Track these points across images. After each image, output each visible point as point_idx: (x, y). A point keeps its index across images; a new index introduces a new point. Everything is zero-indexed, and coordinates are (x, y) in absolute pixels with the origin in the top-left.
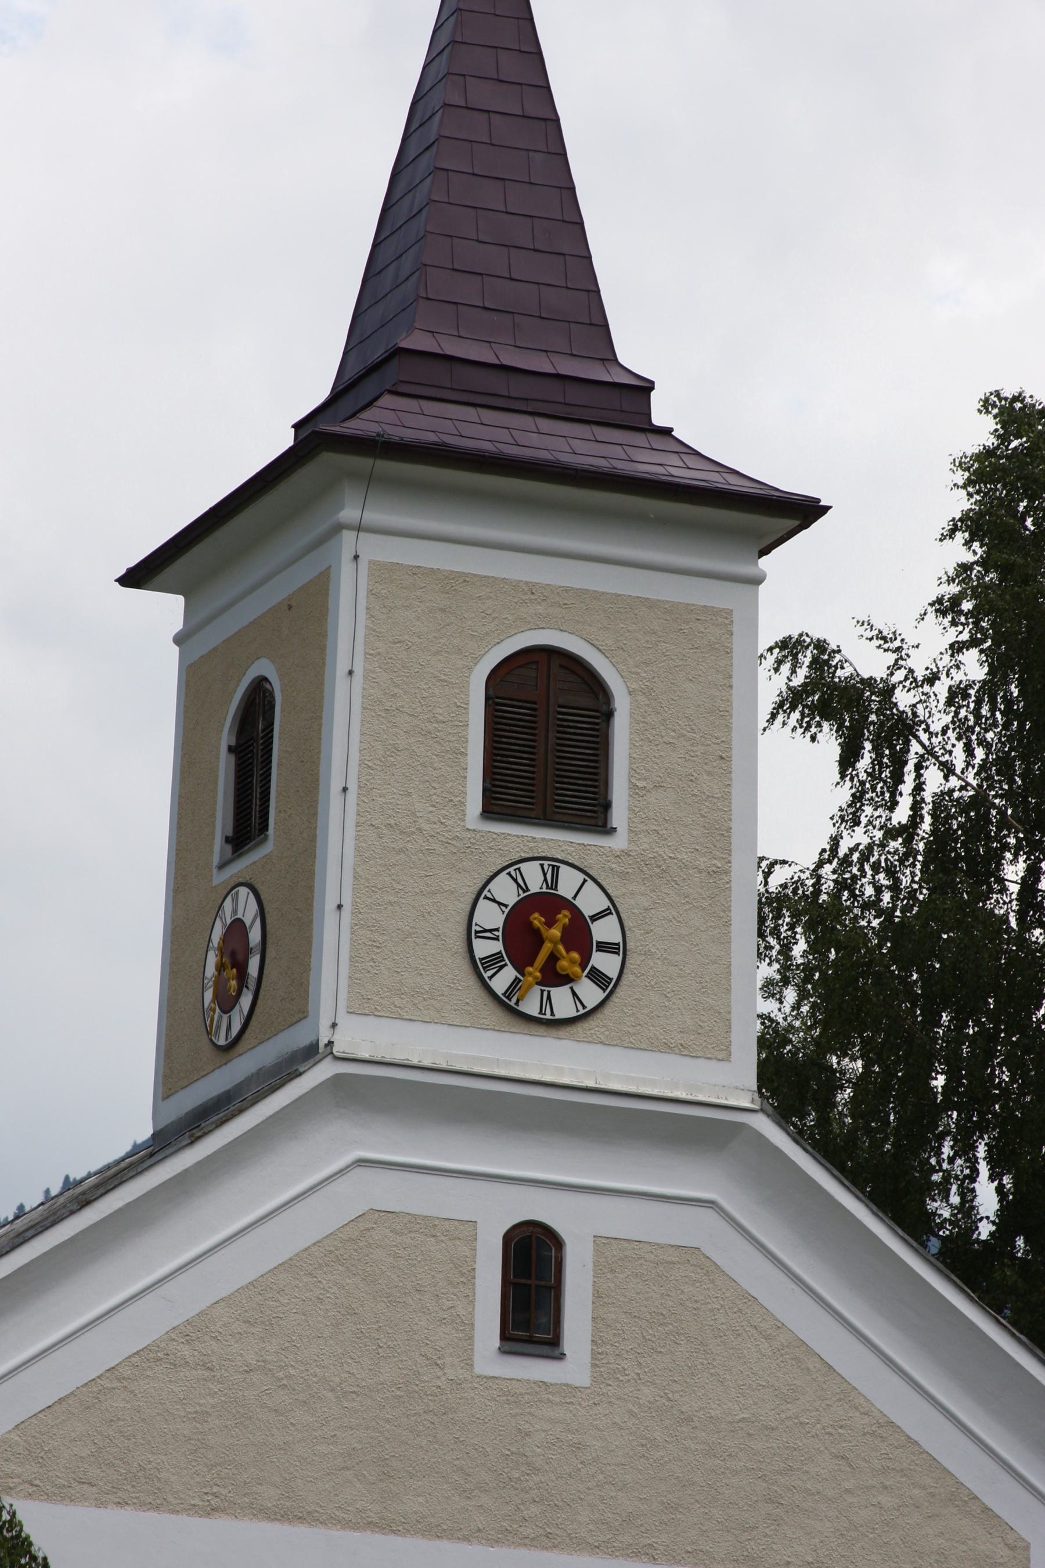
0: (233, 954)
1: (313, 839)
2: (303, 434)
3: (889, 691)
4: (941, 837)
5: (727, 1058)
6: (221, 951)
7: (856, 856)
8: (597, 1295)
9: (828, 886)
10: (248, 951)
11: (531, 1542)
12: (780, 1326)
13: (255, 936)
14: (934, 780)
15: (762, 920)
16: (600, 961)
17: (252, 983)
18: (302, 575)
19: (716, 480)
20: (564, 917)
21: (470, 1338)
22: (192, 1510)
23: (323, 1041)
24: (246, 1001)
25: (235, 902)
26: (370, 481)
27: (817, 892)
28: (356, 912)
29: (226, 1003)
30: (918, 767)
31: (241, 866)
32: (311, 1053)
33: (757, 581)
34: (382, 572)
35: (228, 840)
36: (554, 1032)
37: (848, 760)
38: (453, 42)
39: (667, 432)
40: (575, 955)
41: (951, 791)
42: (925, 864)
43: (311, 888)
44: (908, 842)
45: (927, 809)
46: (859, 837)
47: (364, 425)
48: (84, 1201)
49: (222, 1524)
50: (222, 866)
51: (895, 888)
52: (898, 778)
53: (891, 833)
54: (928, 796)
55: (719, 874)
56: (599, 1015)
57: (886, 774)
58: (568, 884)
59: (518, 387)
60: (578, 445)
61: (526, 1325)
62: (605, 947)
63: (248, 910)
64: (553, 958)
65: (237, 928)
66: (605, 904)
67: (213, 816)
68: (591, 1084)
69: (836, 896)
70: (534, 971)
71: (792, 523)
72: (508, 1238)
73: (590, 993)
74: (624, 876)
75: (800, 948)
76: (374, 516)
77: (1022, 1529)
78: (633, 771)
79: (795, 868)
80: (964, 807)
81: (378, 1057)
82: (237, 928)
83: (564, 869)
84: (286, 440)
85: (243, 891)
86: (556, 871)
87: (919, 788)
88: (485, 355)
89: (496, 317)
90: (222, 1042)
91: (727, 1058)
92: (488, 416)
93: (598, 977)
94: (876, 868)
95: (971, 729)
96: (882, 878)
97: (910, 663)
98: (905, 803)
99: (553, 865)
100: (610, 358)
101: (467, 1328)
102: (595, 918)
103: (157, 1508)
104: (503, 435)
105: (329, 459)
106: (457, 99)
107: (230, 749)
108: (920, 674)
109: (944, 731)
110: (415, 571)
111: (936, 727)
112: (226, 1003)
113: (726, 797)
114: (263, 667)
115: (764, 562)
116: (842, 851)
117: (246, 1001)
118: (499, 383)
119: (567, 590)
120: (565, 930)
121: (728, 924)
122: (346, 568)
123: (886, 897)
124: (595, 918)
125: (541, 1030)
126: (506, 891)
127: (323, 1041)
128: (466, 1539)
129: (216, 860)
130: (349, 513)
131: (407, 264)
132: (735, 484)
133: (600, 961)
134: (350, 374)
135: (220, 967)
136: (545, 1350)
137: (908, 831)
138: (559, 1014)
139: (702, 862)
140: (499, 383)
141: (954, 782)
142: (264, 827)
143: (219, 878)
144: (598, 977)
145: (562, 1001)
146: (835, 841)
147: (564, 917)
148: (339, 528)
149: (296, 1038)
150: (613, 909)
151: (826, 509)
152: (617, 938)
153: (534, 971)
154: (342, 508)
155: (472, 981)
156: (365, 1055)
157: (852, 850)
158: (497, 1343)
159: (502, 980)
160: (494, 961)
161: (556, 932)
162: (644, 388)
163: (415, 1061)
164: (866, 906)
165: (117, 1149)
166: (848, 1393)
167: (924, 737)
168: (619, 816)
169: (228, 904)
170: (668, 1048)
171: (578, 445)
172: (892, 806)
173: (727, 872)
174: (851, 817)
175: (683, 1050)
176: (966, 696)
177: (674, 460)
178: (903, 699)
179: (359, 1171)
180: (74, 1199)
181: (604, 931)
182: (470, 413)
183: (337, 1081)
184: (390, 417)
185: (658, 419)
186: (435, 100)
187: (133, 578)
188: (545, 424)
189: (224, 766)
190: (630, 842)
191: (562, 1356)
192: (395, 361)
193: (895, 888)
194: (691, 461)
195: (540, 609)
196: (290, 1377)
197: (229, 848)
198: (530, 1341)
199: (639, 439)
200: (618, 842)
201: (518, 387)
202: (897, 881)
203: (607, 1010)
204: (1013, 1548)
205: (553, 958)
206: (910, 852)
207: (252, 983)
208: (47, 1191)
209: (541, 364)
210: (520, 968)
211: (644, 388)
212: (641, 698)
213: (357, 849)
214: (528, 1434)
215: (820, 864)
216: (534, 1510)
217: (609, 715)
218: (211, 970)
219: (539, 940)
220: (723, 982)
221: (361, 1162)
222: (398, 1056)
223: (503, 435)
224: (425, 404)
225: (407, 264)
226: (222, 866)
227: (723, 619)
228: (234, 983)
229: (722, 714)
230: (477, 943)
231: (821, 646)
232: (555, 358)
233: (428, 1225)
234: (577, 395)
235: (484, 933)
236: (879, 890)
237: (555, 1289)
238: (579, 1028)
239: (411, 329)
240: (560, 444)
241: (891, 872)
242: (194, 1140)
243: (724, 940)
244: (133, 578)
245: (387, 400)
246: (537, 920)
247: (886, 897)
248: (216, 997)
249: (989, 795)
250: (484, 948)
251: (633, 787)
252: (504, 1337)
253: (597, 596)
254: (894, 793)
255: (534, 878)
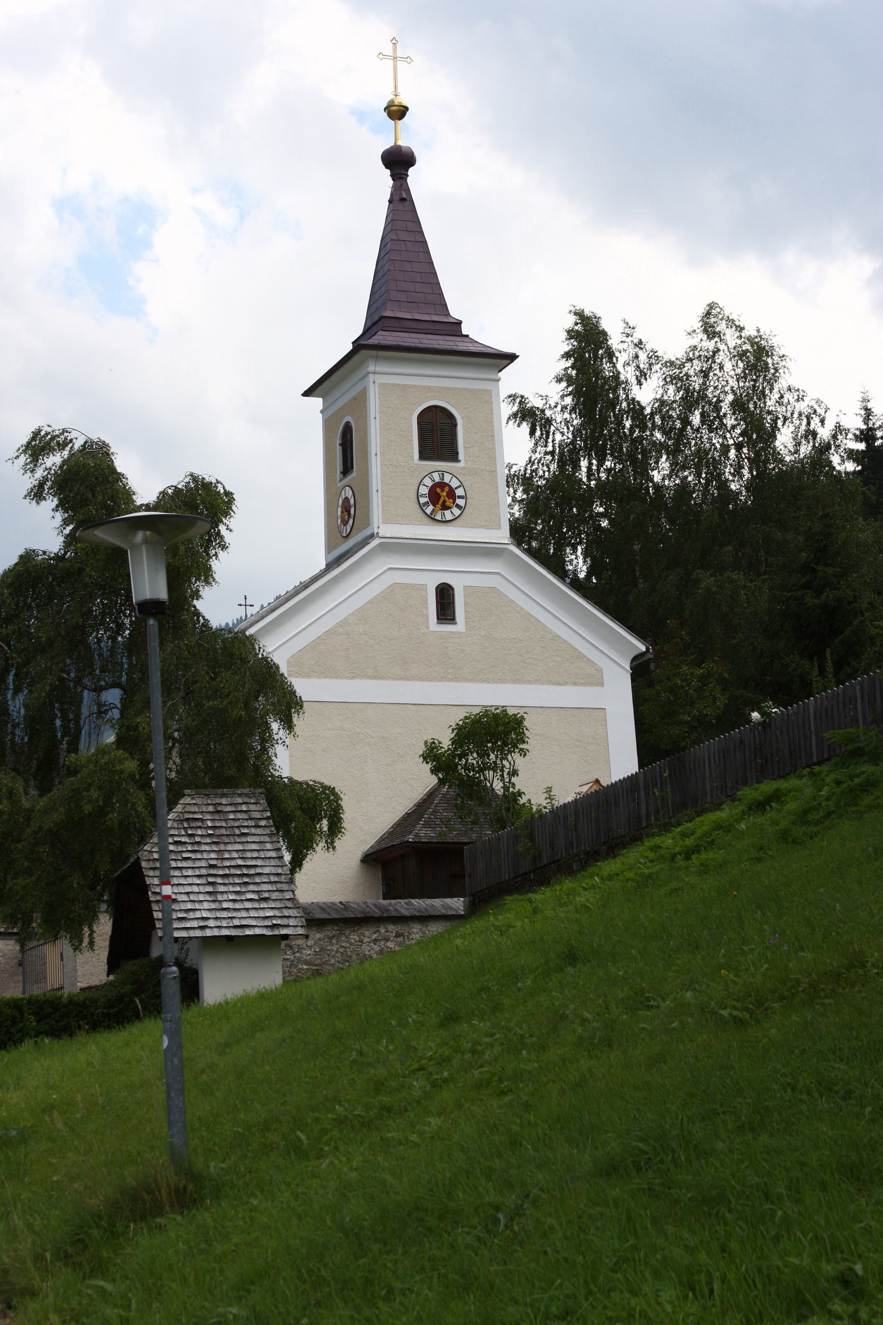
0: (346, 508)
1: (367, 471)
2: (355, 345)
3: (543, 411)
4: (561, 454)
5: (500, 528)
6: (342, 507)
7: (536, 461)
8: (466, 604)
9: (529, 472)
10: (350, 507)
11: (451, 680)
12: (522, 609)
13: (352, 502)
14: (558, 437)
15: (508, 482)
16: (459, 501)
17: (352, 516)
18: (357, 389)
19: (484, 350)
20: (447, 489)
21: (428, 620)
22: (347, 678)
23: (375, 533)
24: (351, 522)
25: (345, 491)
26: (377, 358)
27: (525, 474)
28: (382, 492)
29: (345, 523)
30: (554, 434)
31: (347, 480)
32: (372, 536)
33: (498, 380)
34: (383, 386)
35: (341, 473)
36: (446, 524)
37: (532, 433)
38: (392, 220)
39: (467, 336)
40: (451, 500)
41: (564, 440)
42: (558, 463)
43: (368, 485)
44: (553, 456)
45: (557, 446)
46: (538, 456)
47: (373, 341)
48: (288, 600)
49: (356, 682)
50: (340, 481)
51: (549, 471)
52: (548, 437)
53: (546, 453)
54: (557, 442)
55: (494, 472)
56: (460, 518)
57: (544, 436)
58: (447, 480)
59: (420, 326)
60: (440, 342)
61: (444, 615)
62: (459, 497)
63: (349, 493)
64: (444, 502)
65: (346, 500)
66: (459, 484)
67: (336, 465)
68: (459, 540)
69: (531, 474)
70: (439, 506)
71: (508, 361)
72: (437, 588)
73: (457, 512)
74: (464, 475)
75: (318, 826)
76: (378, 369)
77: (600, 665)
78: (464, 442)
79: (518, 466)
80: (567, 445)
81: (393, 536)
82: (346, 500)
83: (445, 474)
84: (350, 347)
85: (347, 488)
86: (443, 475)
87: (553, 441)
88: (410, 317)
89: (412, 304)
90: (344, 535)
91: (500, 528)
92: (412, 335)
93: (458, 506)
94: (543, 465)
95: (568, 422)
96: (545, 468)
97: (550, 402)
98: (550, 445)
99: (442, 473)
100: (448, 314)
101: (426, 617)
102: (456, 488)
103: (336, 678)
104: (417, 341)
105: (364, 353)
106: (395, 237)
107: (340, 445)
108: (553, 405)
109: (561, 422)
110: (393, 385)
111: (558, 421)
112: (345, 523)
113: (494, 448)
114: (348, 418)
115: (500, 374)
116: (533, 459)
117: (351, 522)
118: (414, 325)
119: (440, 387)
120: (447, 493)
121: (497, 487)
122: (371, 386)
123: (547, 474)
124: (456, 488)
125: (443, 524)
126: (428, 482)
127: (375, 533)
128: (431, 681)
129: (338, 479)
130: (371, 368)
131: (383, 289)
132: (490, 351)
133: (459, 501)
134: (368, 325)
135: (342, 512)
136: (451, 622)
137: (552, 453)
138: (448, 519)
139: (488, 469)
140: (414, 325)
141: (565, 437)
142: (352, 468)
143: (340, 485)
144: (458, 506)
145: (448, 515)
146: (530, 458)
147: (447, 489)
148: (368, 373)
149: (367, 532)
150: (461, 485)
151: (518, 356)
152: (464, 494)
153: (439, 506)
154: (368, 367)
155: (420, 510)
156: (389, 536)
157: (535, 459)
158: (436, 620)
159: (429, 510)
160: (426, 504)
161: (444, 494)
162: (459, 323)
163: (404, 537)
164: (540, 477)
165: (316, 571)
166: (544, 628)
167: (555, 424)
168: (461, 456)
169: (343, 492)
170: (482, 527)
171: (440, 342)
172: (546, 446)
173: (496, 471)
174: (534, 452)
175: (487, 527)
176: (566, 409)
177: (470, 345)
178: (548, 413)
179: (389, 572)
180: (304, 586)
181: (459, 492)
182: (406, 335)
183: (381, 544)
184: (382, 338)
185: (464, 333)
186: (388, 239)
187: (307, 394)
188: (429, 336)
189: (338, 450)
190: (466, 464)
191: (456, 623)
192: (382, 321)
193: (549, 471)
194: (475, 345)
195: (432, 394)
196: (373, 635)
197: (342, 475)
198: (446, 619)
199: (459, 339)
200: (461, 464)
201: (420, 326)
202: (549, 469)
203: (462, 516)
204: (598, 670)
205: (444, 502)
206: (553, 460)
207: (352, 516)
208: (262, 606)
209: (427, 318)
210: (435, 506)
211: (459, 323)
212: (465, 419)
213: (381, 472)
214: (447, 648)
215: (527, 465)
216: (451, 670)
217: (456, 425)
218: (339, 513)
219: (439, 496)
220: (497, 505)
221: (390, 569)
222: (399, 536)
223: (417, 341)
224: (392, 333)
225: (383, 289)
226: (340, 481)
227: (489, 393)
228: (347, 517)
229: (490, 422)
230: (420, 499)
231: (522, 397)
232: (431, 316)
233: (412, 587)
234: (438, 327)
235: (423, 495)
236: (544, 472)
237: (452, 603)
238: (454, 523)
239: (386, 310)
240: (431, 342)
241: (548, 466)
242: (338, 566)
243: (497, 492)
244: (307, 394)
245: (380, 333)
246: (438, 490)
247: (547, 474)
248: (342, 521)
249: (499, 1033)
250: (423, 500)
251: (465, 447)
252: (438, 619)
253: (449, 388)
254: (547, 442)
255: (437, 478)
